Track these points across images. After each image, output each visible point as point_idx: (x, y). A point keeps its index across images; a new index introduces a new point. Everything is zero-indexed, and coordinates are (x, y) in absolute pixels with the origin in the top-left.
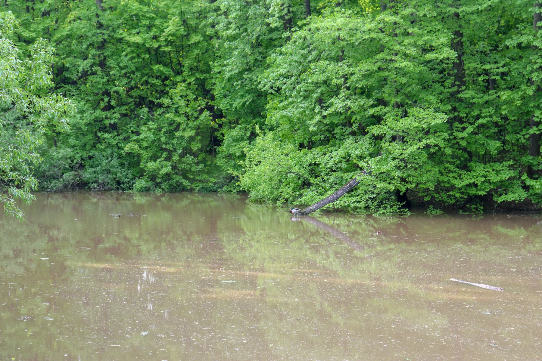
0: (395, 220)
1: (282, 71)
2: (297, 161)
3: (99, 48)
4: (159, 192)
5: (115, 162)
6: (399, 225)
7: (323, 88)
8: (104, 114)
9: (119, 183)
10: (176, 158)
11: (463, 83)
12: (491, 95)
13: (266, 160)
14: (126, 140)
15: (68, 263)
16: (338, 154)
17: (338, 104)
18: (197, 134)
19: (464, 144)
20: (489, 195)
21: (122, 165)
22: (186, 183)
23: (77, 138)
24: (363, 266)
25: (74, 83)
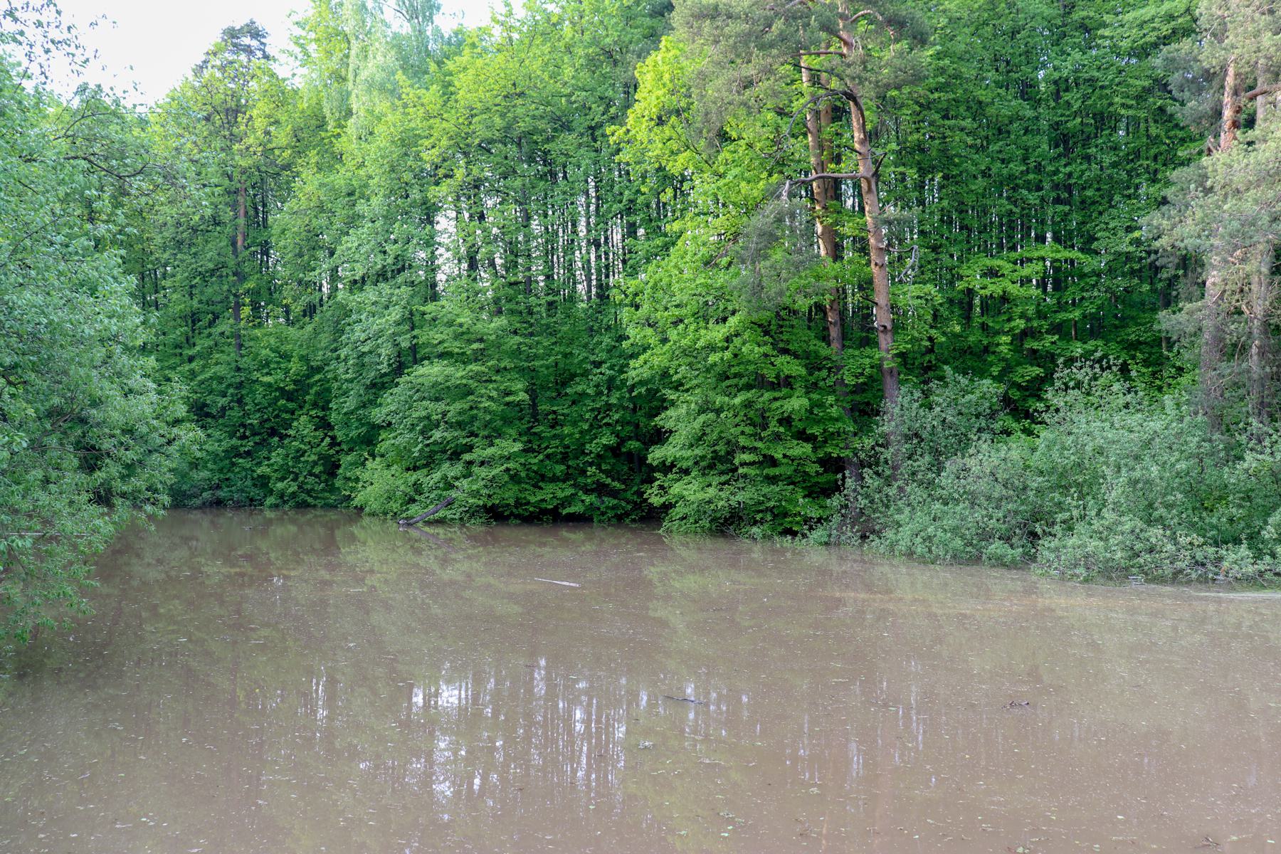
0: (483, 529)
1: (393, 408)
2: (403, 481)
3: (237, 388)
4: (287, 507)
5: (249, 483)
6: (487, 533)
7: (426, 422)
8: (239, 442)
9: (252, 500)
10: (301, 479)
11: (537, 420)
12: (558, 431)
13: (376, 480)
14: (259, 464)
15: (205, 569)
16: (437, 476)
17: (437, 435)
18: (319, 459)
19: (535, 468)
20: (556, 508)
21: (255, 485)
22: (310, 500)
23: (215, 463)
24: (458, 566)
25: (214, 417)
